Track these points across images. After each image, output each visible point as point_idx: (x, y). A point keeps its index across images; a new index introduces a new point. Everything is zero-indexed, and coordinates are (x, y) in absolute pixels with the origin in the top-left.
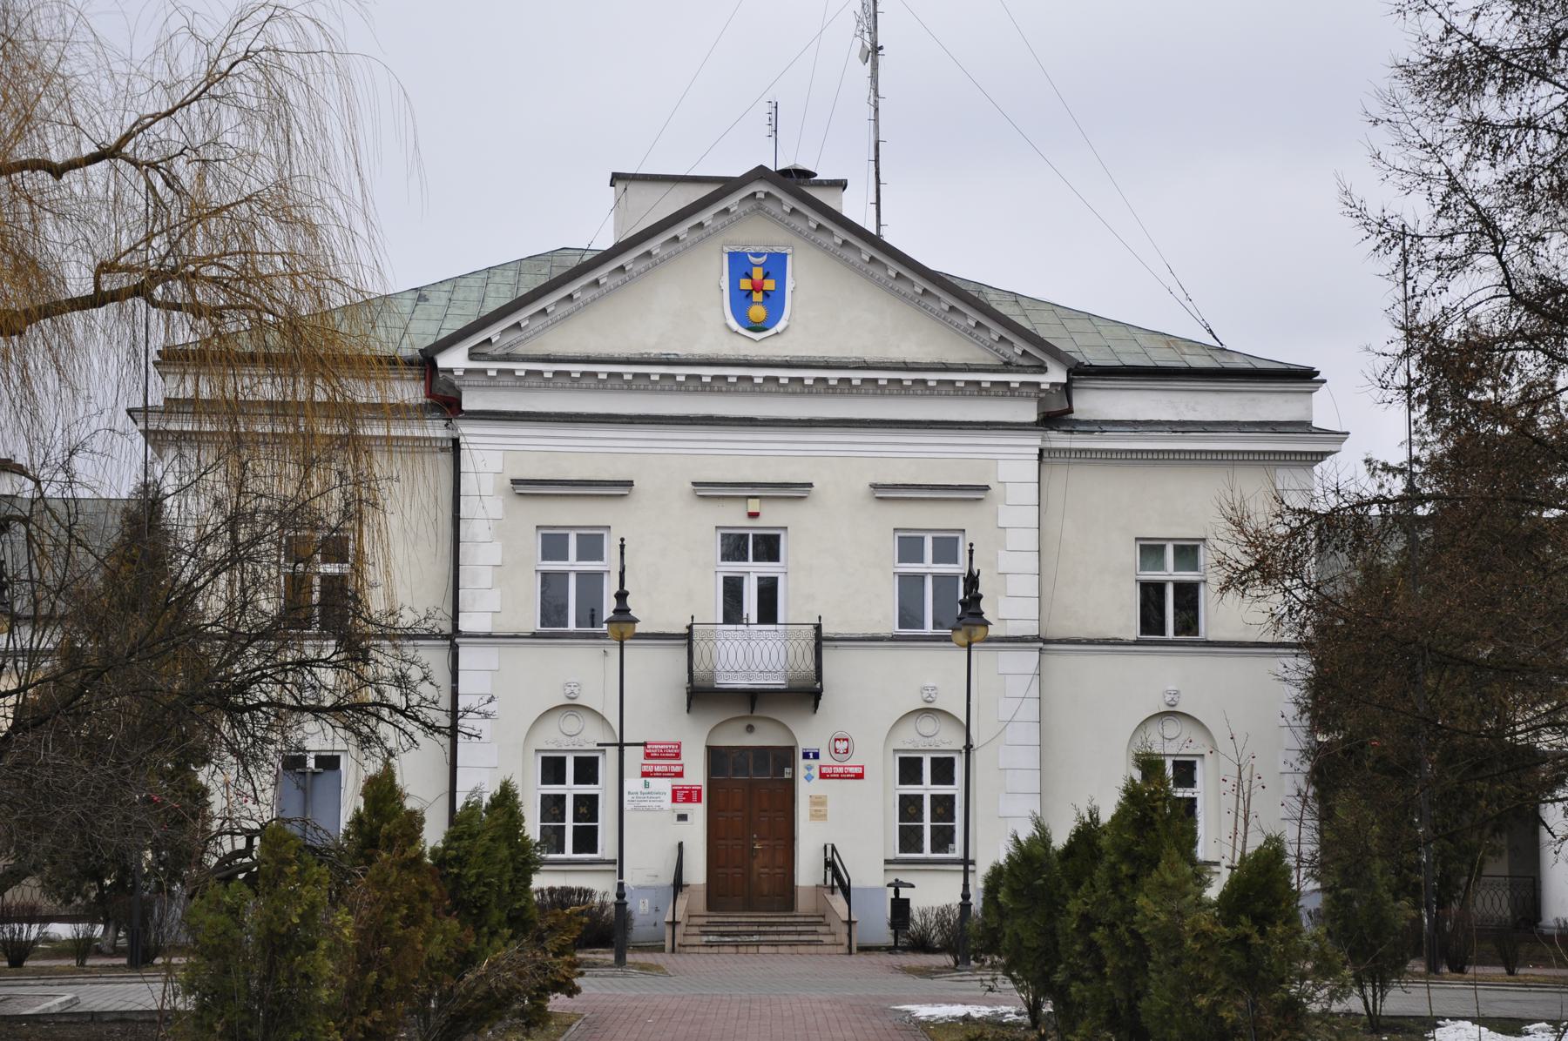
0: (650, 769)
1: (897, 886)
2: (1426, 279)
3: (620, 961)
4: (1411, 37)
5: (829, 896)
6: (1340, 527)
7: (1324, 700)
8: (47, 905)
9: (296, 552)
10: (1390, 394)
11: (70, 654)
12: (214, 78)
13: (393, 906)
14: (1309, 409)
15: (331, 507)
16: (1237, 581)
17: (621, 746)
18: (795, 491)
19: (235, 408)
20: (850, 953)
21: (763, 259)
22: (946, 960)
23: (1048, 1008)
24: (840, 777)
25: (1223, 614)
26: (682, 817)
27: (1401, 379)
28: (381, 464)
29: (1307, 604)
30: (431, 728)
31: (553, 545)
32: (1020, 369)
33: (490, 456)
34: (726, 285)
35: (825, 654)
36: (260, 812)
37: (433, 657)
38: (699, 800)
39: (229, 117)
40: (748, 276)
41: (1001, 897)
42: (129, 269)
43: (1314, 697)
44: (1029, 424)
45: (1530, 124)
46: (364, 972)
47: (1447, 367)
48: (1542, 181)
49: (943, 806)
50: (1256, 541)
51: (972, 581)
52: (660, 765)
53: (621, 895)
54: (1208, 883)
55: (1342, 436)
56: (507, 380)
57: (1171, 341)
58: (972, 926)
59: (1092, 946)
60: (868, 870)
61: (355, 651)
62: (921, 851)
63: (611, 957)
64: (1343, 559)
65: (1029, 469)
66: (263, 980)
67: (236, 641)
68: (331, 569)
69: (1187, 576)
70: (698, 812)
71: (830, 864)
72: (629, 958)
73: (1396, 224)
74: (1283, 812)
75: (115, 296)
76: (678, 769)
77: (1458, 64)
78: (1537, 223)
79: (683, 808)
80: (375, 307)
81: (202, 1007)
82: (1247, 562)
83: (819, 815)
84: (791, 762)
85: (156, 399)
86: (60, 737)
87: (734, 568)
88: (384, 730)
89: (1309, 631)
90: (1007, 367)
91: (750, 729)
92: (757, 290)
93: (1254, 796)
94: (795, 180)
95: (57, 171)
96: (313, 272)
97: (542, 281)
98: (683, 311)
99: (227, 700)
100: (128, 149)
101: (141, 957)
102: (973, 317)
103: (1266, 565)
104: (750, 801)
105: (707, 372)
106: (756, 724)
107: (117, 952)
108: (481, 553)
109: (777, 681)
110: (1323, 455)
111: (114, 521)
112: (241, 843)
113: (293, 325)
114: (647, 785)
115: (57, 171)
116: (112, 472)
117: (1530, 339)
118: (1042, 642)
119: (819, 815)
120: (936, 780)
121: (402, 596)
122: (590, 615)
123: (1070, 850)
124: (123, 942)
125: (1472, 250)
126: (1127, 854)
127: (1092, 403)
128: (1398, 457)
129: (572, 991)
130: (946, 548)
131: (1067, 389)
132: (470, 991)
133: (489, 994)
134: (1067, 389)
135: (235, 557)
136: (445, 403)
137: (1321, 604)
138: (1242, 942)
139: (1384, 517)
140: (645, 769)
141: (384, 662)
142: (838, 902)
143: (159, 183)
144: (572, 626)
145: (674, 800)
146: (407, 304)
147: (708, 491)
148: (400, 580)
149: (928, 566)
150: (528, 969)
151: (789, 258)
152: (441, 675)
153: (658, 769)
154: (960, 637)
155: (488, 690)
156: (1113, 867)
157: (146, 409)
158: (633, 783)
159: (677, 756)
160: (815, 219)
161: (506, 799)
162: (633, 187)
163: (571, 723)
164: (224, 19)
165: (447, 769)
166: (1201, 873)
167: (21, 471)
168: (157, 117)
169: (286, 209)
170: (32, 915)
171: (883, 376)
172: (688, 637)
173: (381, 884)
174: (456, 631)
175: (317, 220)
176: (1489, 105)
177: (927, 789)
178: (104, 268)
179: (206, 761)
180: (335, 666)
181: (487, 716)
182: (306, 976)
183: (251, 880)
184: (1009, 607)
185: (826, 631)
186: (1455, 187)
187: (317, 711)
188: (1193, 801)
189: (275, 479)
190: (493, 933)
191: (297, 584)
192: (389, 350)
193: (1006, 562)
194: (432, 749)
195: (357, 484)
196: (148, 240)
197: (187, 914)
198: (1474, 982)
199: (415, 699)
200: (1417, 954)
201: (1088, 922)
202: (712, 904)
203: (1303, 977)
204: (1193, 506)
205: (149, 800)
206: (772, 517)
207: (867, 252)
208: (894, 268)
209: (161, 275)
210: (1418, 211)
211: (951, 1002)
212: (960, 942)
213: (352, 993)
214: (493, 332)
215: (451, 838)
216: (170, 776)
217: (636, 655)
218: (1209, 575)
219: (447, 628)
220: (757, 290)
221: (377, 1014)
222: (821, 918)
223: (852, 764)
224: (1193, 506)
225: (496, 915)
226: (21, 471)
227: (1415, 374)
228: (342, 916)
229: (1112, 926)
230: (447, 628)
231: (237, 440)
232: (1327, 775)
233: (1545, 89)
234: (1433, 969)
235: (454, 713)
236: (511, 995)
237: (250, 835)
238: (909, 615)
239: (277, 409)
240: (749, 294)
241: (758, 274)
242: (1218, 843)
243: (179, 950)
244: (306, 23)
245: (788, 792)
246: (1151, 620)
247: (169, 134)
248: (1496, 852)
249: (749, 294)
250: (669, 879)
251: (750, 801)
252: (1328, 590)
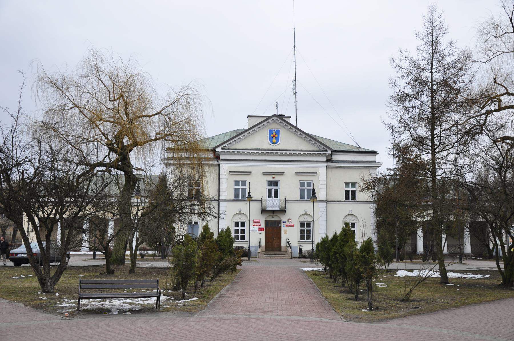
1: (300, 246)
2: (397, 135)
3: (249, 259)
4: (393, 92)
6: (381, 180)
7: (379, 212)
8: (147, 248)
9: (190, 185)
10: (390, 156)
11: (151, 203)
12: (177, 99)
13: (208, 249)
15: (197, 176)
16: (363, 190)
17: (249, 220)
18: (281, 174)
19: (181, 158)
22: (309, 260)
23: (328, 268)
25: (360, 196)
27: (392, 153)
28: (206, 169)
29: (376, 194)
30: (215, 217)
31: (237, 183)
32: (323, 151)
33: (225, 167)
36: (184, 232)
37: (215, 204)
39: (180, 106)
41: (319, 248)
42: (162, 134)
43: (377, 211)
45: (414, 107)
46: (203, 261)
47: (401, 151)
48: (417, 117)
49: (309, 232)
50: (366, 183)
51: (314, 190)
52: (256, 224)
53: (249, 248)
54: (357, 246)
55: (381, 163)
56: (229, 153)
57: (350, 146)
58: (314, 253)
59: (336, 258)
60: (295, 244)
61: (201, 203)
63: (248, 259)
64: (382, 186)
65: (325, 169)
66: (186, 262)
67: (180, 201)
68: (197, 188)
70: (263, 232)
71: (288, 242)
72: (251, 259)
73: (391, 125)
74: (371, 233)
75: (159, 139)
77: (401, 96)
78: (416, 125)
79: (261, 232)
80: (204, 140)
81: (175, 267)
82: (365, 187)
83: (285, 233)
84: (281, 224)
85: (166, 157)
86: (149, 217)
87: (270, 188)
88: (206, 217)
89: (376, 199)
90: (320, 151)
91: (273, 217)
92: (274, 137)
93: (365, 231)
94: (281, 116)
95: (149, 117)
96: (193, 134)
97: (235, 135)
98: (261, 140)
99: (179, 212)
100: (162, 112)
101: (164, 257)
102: (314, 141)
103: (368, 187)
104: (273, 231)
105: (265, 152)
107: (160, 256)
108: (224, 185)
109: (278, 209)
110: (378, 167)
111: (158, 178)
112: (181, 237)
113: (190, 143)
115: (150, 117)
116: (157, 171)
117: (415, 146)
118: (327, 201)
119: (285, 233)
121: (210, 193)
122: (244, 196)
123: (332, 240)
124: (160, 255)
125: (405, 130)
126: (343, 241)
127: (336, 157)
128: (392, 168)
129: (241, 265)
130: (309, 184)
131: (331, 155)
132: (222, 265)
133: (226, 265)
134: (331, 155)
135: (180, 186)
136: (217, 157)
137: (378, 194)
138: (364, 256)
139: (390, 178)
141: (207, 205)
142: (289, 249)
143: (167, 119)
144: (240, 198)
146: (210, 140)
147: (265, 173)
148: (209, 189)
149: (306, 187)
150: (232, 261)
152: (217, 207)
154: (312, 200)
155: (225, 210)
156: (340, 243)
157: (164, 159)
158: (251, 227)
160: (285, 124)
161: (228, 230)
162: (251, 118)
163: (240, 216)
164: (179, 89)
165: (295, 199)
166: (356, 244)
167: (143, 170)
168: (167, 107)
169: (189, 123)
170: (145, 249)
171: (297, 152)
172: (262, 200)
173: (206, 245)
174: (219, 199)
175: (195, 124)
176: (407, 104)
177: (306, 228)
178: (157, 134)
179: (174, 222)
180: (198, 205)
181: (225, 215)
182: (193, 261)
183: (183, 244)
184: (321, 195)
185: (287, 199)
186: (402, 118)
187: (194, 214)
188: (354, 231)
189: (187, 172)
190: (226, 254)
191: (190, 191)
192: (207, 148)
193: (320, 186)
194: (215, 220)
195: (202, 172)
196: (165, 129)
197: (172, 250)
198: (405, 263)
199: (212, 212)
200: (395, 258)
201: (335, 253)
202: (266, 249)
203: (375, 263)
204: (355, 176)
205: (165, 229)
206: (277, 178)
207: (294, 130)
208: (299, 133)
209: (167, 135)
210: (395, 123)
211: (310, 267)
212: (312, 256)
213: (201, 265)
214: (226, 145)
215: (218, 237)
216: (168, 225)
217: (252, 203)
218: (357, 189)
219: (217, 199)
220: (274, 137)
221: (206, 269)
222: (286, 252)
223: (292, 224)
224: (355, 176)
225: (227, 251)
226: (143, 170)
227: (395, 152)
228: (199, 251)
229: (340, 254)
230: (217, 199)
231: (180, 165)
232: (379, 226)
233: (417, 101)
234: (398, 261)
235: (219, 214)
236: (230, 265)
237: (183, 236)
238: (302, 197)
239: (187, 159)
241: (274, 134)
242: (359, 238)
243: (170, 256)
244: (194, 90)
245: (280, 228)
246: (347, 197)
247: (169, 109)
248: (409, 239)
250: (258, 245)
251: (273, 231)
252: (379, 192)
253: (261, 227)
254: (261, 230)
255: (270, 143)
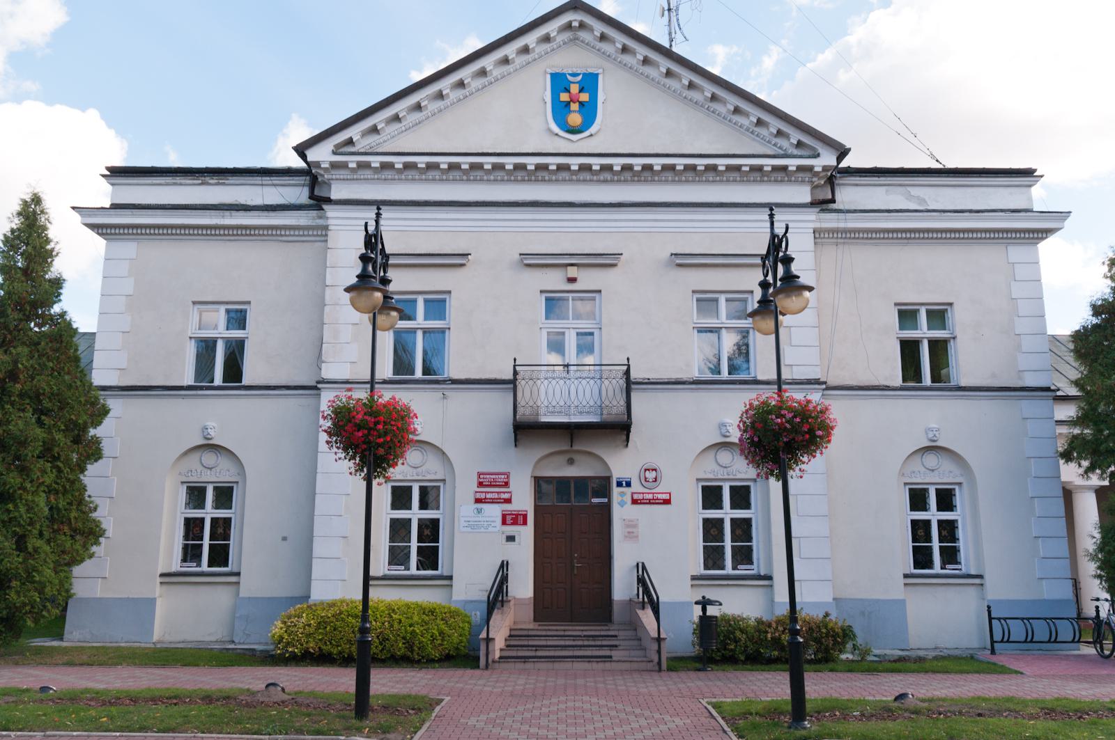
0: (483, 496)
5: (640, 612)
14: (1030, 199)
20: (660, 670)
21: (580, 78)
24: (650, 502)
26: (511, 539)
34: (548, 98)
35: (634, 395)
38: (525, 523)
40: (567, 90)
44: (808, 203)
52: (492, 493)
62: (723, 568)
69: (938, 334)
70: (526, 534)
71: (641, 581)
76: (506, 496)
79: (511, 530)
83: (631, 536)
91: (571, 462)
92: (574, 101)
98: (513, 117)
104: (574, 526)
106: (576, 457)
110: (1047, 232)
114: (479, 511)
120: (734, 506)
140: (478, 496)
142: (647, 617)
144: (419, 373)
145: (504, 522)
151: (600, 77)
153: (489, 496)
159: (506, 484)
177: (727, 513)
185: (634, 375)
207: (665, 64)
214: (354, 132)
220: (574, 101)
223: (661, 489)
240: (568, 104)
241: (574, 89)
245: (605, 513)
249: (568, 104)
251: (574, 526)
253: (515, 507)
254: (515, 522)
255: (556, 129)
